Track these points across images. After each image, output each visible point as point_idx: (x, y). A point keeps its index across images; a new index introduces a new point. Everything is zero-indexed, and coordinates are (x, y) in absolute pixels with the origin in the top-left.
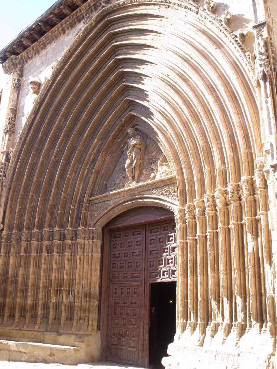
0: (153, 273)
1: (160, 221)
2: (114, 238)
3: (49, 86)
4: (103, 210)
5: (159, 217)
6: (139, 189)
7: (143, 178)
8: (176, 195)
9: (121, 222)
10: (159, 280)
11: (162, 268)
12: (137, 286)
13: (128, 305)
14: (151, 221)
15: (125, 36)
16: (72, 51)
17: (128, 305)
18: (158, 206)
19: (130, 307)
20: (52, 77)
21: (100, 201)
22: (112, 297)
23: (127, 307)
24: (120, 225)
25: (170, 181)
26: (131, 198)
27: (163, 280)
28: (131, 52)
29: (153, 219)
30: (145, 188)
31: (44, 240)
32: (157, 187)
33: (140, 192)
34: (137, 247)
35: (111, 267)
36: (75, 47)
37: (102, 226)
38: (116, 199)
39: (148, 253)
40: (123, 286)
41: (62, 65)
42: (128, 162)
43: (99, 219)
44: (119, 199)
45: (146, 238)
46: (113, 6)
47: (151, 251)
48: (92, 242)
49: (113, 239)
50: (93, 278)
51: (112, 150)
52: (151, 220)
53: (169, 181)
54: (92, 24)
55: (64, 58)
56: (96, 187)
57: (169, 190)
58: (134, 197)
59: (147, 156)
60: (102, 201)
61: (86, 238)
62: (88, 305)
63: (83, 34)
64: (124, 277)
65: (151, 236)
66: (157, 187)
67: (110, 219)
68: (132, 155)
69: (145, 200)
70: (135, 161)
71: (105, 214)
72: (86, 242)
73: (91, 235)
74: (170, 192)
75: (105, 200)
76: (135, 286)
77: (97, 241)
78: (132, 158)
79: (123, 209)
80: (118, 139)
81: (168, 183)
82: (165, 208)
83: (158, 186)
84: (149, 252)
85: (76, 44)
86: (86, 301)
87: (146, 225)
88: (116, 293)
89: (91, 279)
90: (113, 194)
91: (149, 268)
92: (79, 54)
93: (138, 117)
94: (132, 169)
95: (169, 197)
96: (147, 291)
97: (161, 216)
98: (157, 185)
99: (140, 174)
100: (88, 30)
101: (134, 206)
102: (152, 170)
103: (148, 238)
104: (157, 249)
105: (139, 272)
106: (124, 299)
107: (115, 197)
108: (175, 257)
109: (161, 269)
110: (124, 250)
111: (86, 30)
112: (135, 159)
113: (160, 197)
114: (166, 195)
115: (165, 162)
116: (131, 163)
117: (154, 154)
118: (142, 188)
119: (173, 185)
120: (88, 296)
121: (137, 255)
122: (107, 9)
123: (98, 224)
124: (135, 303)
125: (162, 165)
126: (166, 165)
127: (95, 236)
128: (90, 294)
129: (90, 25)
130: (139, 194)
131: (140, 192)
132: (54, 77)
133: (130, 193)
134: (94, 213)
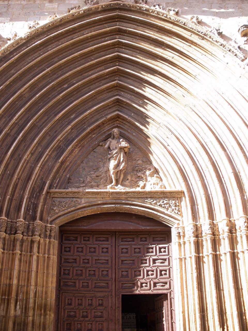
0: (125, 284)
1: (132, 231)
2: (66, 240)
3: (20, 44)
4: (69, 207)
5: (158, 228)
6: (130, 194)
7: (127, 183)
8: (177, 209)
9: (85, 225)
10: (137, 292)
11: (141, 279)
12: (102, 297)
13: (91, 319)
14: (131, 230)
15: (133, 39)
16: (63, 22)
17: (91, 319)
18: (147, 216)
19: (93, 321)
20: (28, 37)
21: (65, 196)
22: (64, 310)
23: (88, 321)
24: (85, 228)
25: (172, 194)
26: (114, 201)
27: (142, 292)
28: (138, 56)
29: (134, 228)
30: (137, 194)
31: (18, 233)
32: (153, 197)
33: (128, 198)
34: (103, 254)
35: (62, 273)
36: (68, 20)
37: (61, 224)
38: (91, 199)
39: (118, 262)
40: (83, 297)
41: (45, 30)
42: (113, 163)
43: (60, 216)
44: (95, 200)
45: (117, 246)
46: (133, 6)
47: (122, 261)
48: (49, 241)
49: (64, 242)
50: (50, 285)
51: (83, 143)
52: (131, 228)
53: (169, 194)
54: (98, 8)
55: (50, 24)
56: (57, 179)
57: (169, 203)
58: (119, 201)
59: (131, 162)
60: (67, 196)
61: (42, 236)
63: (84, 11)
64: (83, 286)
65: (122, 245)
66: (153, 197)
67: (74, 219)
68: (120, 157)
69: (133, 207)
70: (123, 164)
71: (72, 211)
72: (42, 241)
73: (48, 233)
74: (170, 206)
75: (73, 196)
76: (100, 297)
77: (55, 241)
78: (119, 160)
79: (97, 211)
80: (93, 135)
81: (168, 196)
82: (159, 220)
83: (155, 196)
84: (120, 261)
85: (71, 19)
86: (41, 315)
87: (115, 232)
88: (70, 304)
89: (47, 287)
90: (88, 193)
91: (121, 279)
92: (71, 30)
93: (129, 122)
94: (118, 171)
95: (168, 209)
96: (119, 303)
97: (145, 226)
98: (155, 195)
99: (125, 179)
100: (91, 12)
101: (114, 210)
102: (140, 178)
103: (118, 246)
104: (132, 259)
105: (107, 282)
106: (83, 312)
107: (90, 196)
108: (157, 269)
109: (139, 280)
110: (83, 256)
111: (88, 11)
112: (123, 162)
113: (156, 208)
114: (164, 207)
115: (155, 174)
116: (118, 165)
117: (140, 162)
118: (133, 194)
119: (173, 199)
120: (43, 308)
121: (102, 263)
122: (124, 5)
123: (57, 221)
124: (101, 317)
125: (152, 175)
126: (157, 177)
127: (53, 234)
128: (46, 305)
129: (96, 8)
130: (126, 199)
131: (128, 198)
132: (29, 38)
133: (115, 195)
134: (55, 208)
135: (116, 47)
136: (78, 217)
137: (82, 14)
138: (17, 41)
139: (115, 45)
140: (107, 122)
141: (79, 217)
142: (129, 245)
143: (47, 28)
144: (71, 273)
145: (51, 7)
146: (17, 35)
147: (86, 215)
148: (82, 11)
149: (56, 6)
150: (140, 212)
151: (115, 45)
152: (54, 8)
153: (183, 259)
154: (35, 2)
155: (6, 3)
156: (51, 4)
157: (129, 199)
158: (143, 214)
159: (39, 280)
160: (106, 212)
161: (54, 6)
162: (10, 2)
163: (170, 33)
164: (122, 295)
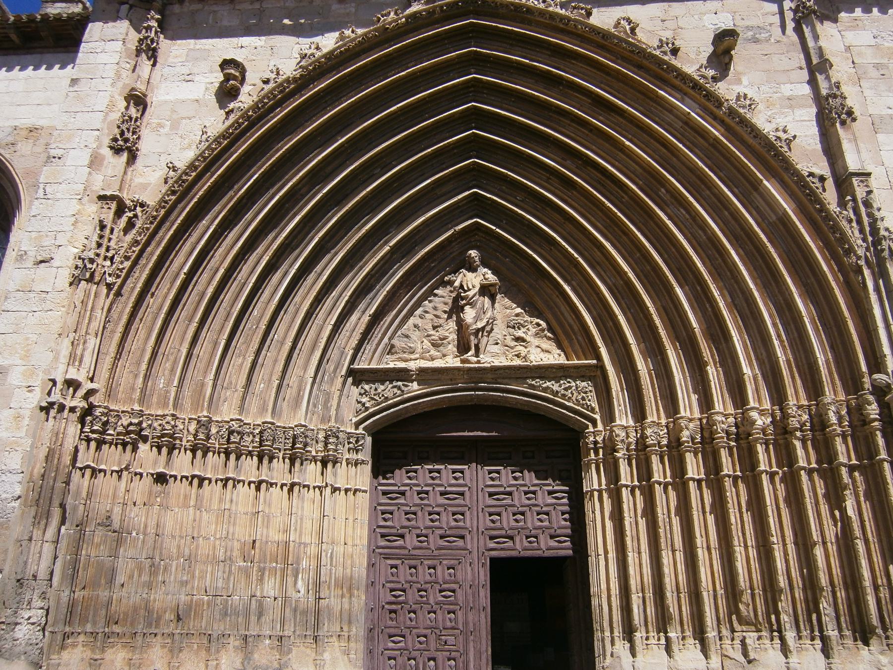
62: (346, 606)
86: (343, 596)
135: (470, 92)
136: (407, 416)
137: (404, 25)
138: (281, 84)
139: (468, 87)
140: (456, 240)
141: (410, 415)
142: (396, 504)
143: (336, 57)
144: (460, 509)
145: (342, 11)
146: (281, 73)
147: (422, 411)
148: (404, 20)
149: (353, 10)
150: (521, 404)
151: (468, 87)
152: (348, 14)
153: (596, 494)
154: (311, 2)
155: (257, 6)
156: (343, 6)
157: (499, 381)
158: (526, 408)
159: (255, 174)
160: (459, 404)
161: (348, 11)
162: (264, 5)
163: (575, 59)
164: (493, 560)
